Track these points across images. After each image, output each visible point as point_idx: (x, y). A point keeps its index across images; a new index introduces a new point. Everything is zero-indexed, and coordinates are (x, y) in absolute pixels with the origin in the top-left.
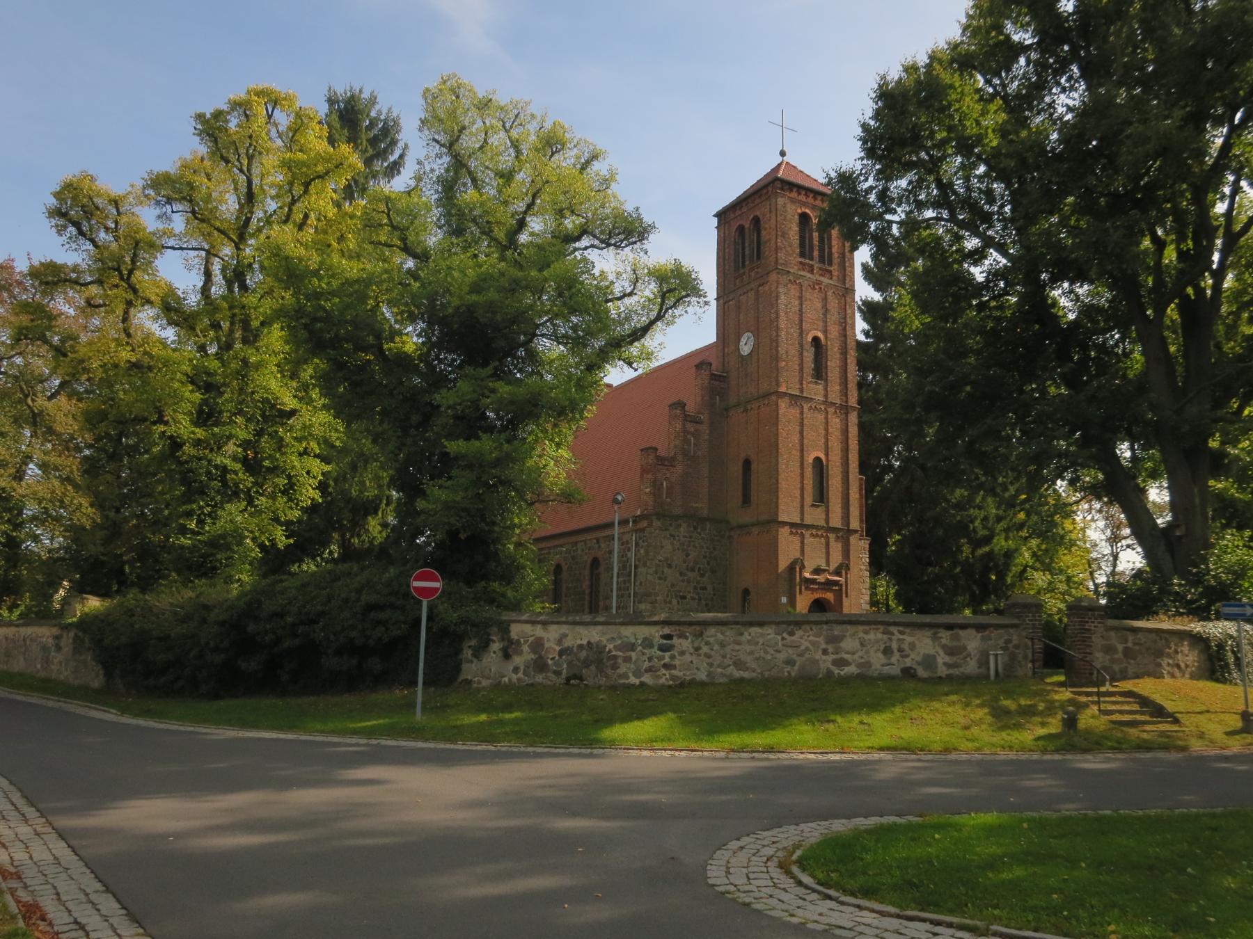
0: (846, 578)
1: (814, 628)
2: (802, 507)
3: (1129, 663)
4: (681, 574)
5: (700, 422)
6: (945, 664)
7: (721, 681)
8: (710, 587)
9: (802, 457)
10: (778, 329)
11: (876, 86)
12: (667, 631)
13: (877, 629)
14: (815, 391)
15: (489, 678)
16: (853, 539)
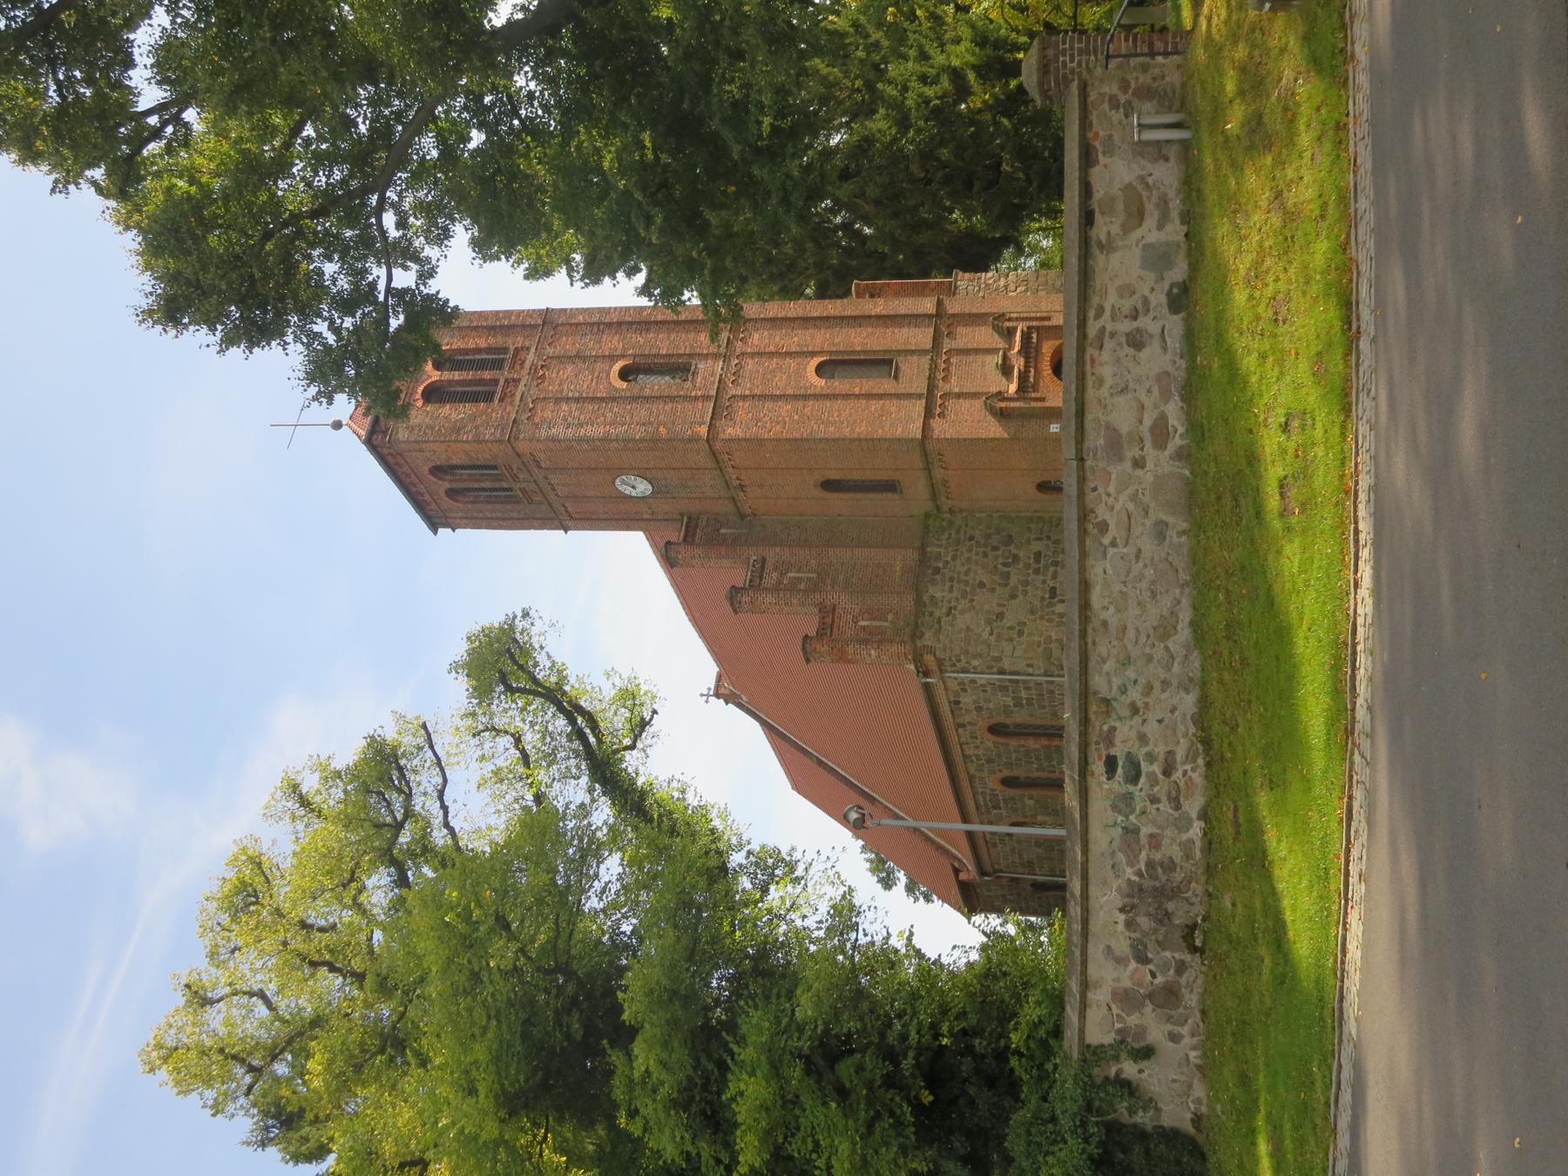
0: (1017, 319)
2: (898, 396)
4: (1013, 597)
5: (764, 561)
6: (1160, 227)
7: (1197, 664)
8: (1036, 546)
9: (816, 397)
10: (606, 439)
11: (159, 328)
12: (1098, 767)
13: (1093, 361)
14: (708, 372)
15: (1190, 1086)
16: (953, 306)
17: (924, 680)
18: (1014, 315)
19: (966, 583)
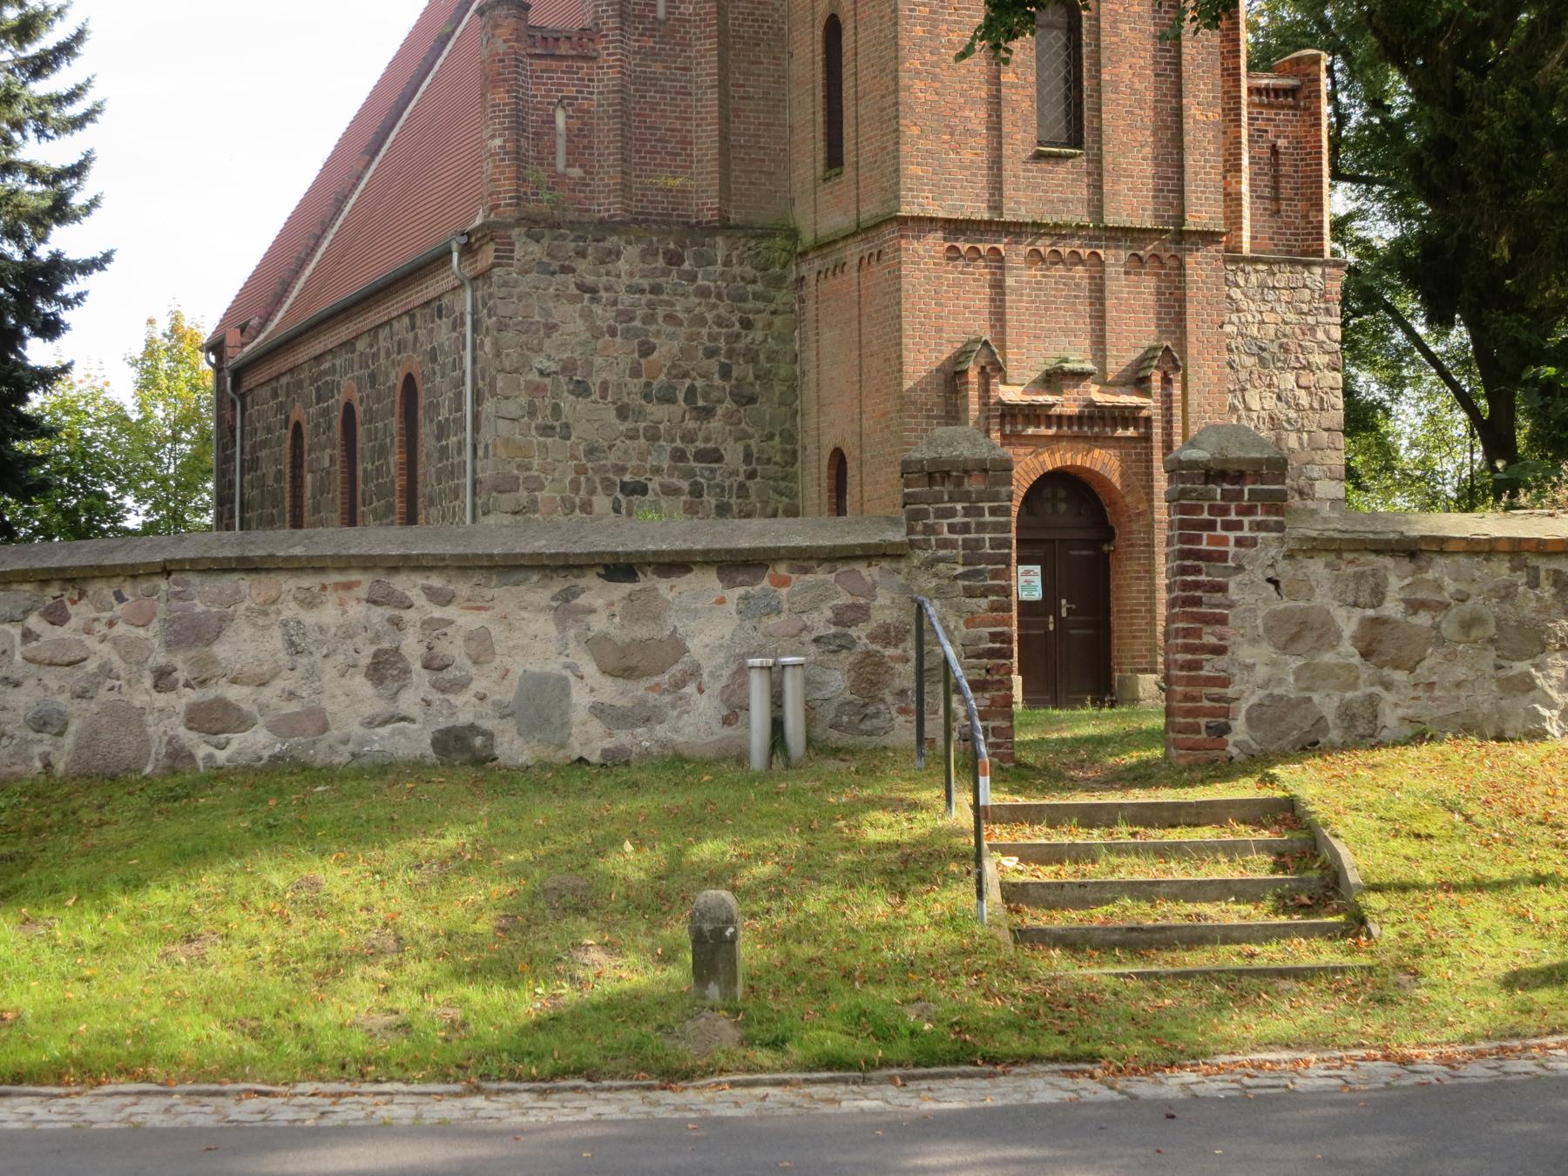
0: (1167, 396)
1: (127, 590)
2: (996, 163)
3: (1388, 685)
4: (622, 413)
6: (598, 710)
8: (733, 454)
13: (348, 586)
17: (455, 246)
18: (1176, 390)
19: (649, 319)
